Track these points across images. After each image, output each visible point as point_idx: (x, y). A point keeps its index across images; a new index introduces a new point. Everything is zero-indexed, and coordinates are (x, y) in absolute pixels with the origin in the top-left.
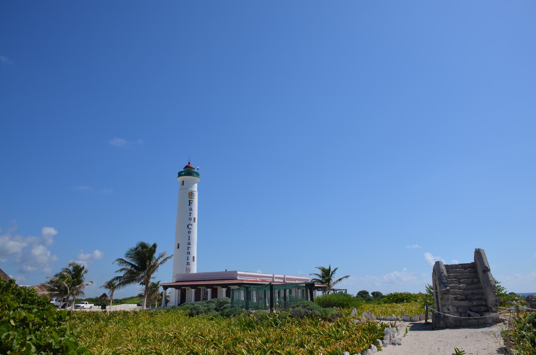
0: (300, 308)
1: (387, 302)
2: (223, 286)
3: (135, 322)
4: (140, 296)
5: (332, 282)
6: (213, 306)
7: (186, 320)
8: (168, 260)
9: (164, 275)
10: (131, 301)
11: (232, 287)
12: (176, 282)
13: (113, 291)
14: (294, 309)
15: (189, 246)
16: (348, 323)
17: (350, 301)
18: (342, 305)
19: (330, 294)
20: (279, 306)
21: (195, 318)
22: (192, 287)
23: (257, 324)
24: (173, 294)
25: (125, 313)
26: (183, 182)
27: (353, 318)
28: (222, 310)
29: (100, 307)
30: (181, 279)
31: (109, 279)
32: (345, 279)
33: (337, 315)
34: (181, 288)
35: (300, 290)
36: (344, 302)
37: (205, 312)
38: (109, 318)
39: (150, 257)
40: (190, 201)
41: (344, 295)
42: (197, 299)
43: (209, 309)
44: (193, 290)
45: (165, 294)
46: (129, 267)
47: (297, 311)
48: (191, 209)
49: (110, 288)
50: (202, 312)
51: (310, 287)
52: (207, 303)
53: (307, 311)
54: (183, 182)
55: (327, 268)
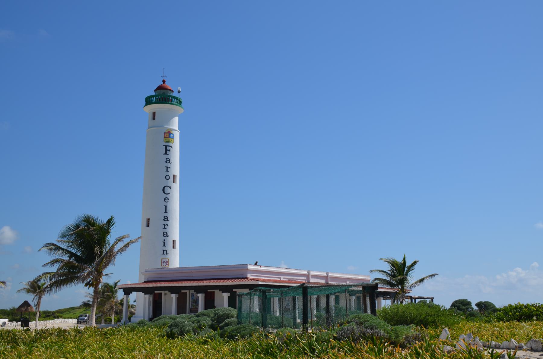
0: (353, 324)
1: (502, 320)
2: (224, 289)
3: (77, 347)
4: (86, 305)
5: (407, 285)
6: (208, 321)
7: (162, 344)
8: (132, 246)
9: (124, 270)
10: (71, 315)
11: (239, 291)
12: (145, 282)
13: (40, 298)
14: (343, 326)
15: (166, 223)
16: (433, 351)
17: (438, 316)
18: (424, 323)
19: (404, 303)
20: (318, 322)
21: (178, 341)
22: (172, 290)
23: (281, 351)
24: (140, 302)
25: (61, 333)
26: (154, 114)
27: (444, 343)
28: (222, 328)
29: (20, 323)
30: (152, 277)
31: (32, 278)
32: (429, 279)
33: (416, 338)
34: (154, 291)
35: (354, 297)
36: (428, 317)
37: (194, 331)
38: (34, 341)
39: (101, 242)
40: (166, 146)
41: (427, 304)
42: (181, 309)
43: (200, 327)
44: (174, 296)
45: (128, 301)
46: (66, 257)
47: (348, 330)
48: (168, 161)
49: (34, 292)
50: (188, 331)
51: (371, 291)
52: (198, 316)
53: (365, 329)
54: (154, 114)
55: (400, 260)
